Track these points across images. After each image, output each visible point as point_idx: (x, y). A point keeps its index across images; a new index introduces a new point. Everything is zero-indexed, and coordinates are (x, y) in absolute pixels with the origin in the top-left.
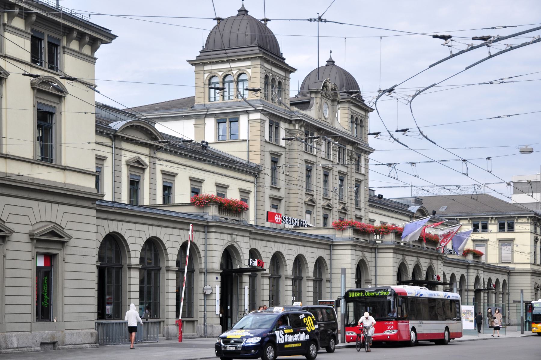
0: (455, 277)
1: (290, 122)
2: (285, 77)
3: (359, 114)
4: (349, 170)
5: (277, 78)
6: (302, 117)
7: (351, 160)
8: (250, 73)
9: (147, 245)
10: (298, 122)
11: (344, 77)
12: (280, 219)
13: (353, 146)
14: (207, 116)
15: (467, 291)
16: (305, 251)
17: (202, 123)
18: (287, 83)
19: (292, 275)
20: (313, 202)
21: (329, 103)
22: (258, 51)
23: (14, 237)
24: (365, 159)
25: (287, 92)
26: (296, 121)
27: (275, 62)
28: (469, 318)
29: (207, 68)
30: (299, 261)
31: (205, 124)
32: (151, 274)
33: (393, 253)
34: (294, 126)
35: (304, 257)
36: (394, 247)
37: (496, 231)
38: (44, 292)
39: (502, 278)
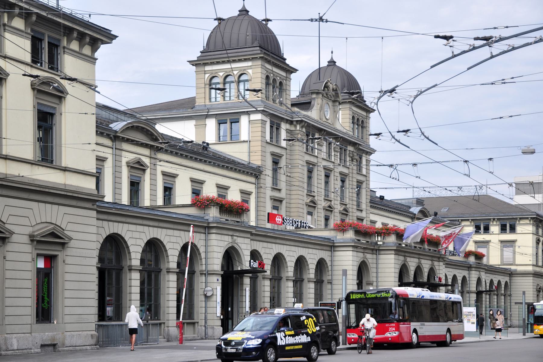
0: (457, 278)
1: (291, 123)
2: (287, 77)
3: (360, 115)
4: (351, 171)
5: (278, 78)
6: (303, 117)
7: (352, 160)
8: (251, 74)
9: (148, 247)
10: (299, 123)
11: (345, 78)
12: (281, 220)
13: (354, 147)
14: (207, 116)
15: (469, 293)
16: (306, 252)
17: (203, 124)
18: (288, 84)
19: (294, 277)
20: (315, 203)
21: (330, 103)
22: (259, 52)
23: (14, 238)
24: (366, 160)
25: (288, 92)
26: (297, 121)
27: (276, 62)
28: (471, 320)
29: (207, 68)
30: (300, 262)
31: (206, 125)
32: (151, 275)
33: (394, 254)
34: (295, 126)
35: (305, 259)
36: (395, 248)
37: (498, 233)
38: (44, 294)
39: (504, 279)
